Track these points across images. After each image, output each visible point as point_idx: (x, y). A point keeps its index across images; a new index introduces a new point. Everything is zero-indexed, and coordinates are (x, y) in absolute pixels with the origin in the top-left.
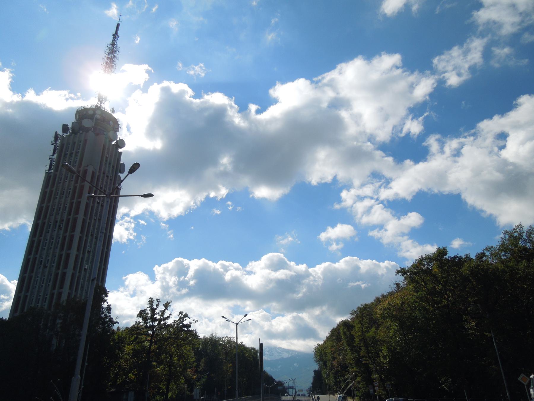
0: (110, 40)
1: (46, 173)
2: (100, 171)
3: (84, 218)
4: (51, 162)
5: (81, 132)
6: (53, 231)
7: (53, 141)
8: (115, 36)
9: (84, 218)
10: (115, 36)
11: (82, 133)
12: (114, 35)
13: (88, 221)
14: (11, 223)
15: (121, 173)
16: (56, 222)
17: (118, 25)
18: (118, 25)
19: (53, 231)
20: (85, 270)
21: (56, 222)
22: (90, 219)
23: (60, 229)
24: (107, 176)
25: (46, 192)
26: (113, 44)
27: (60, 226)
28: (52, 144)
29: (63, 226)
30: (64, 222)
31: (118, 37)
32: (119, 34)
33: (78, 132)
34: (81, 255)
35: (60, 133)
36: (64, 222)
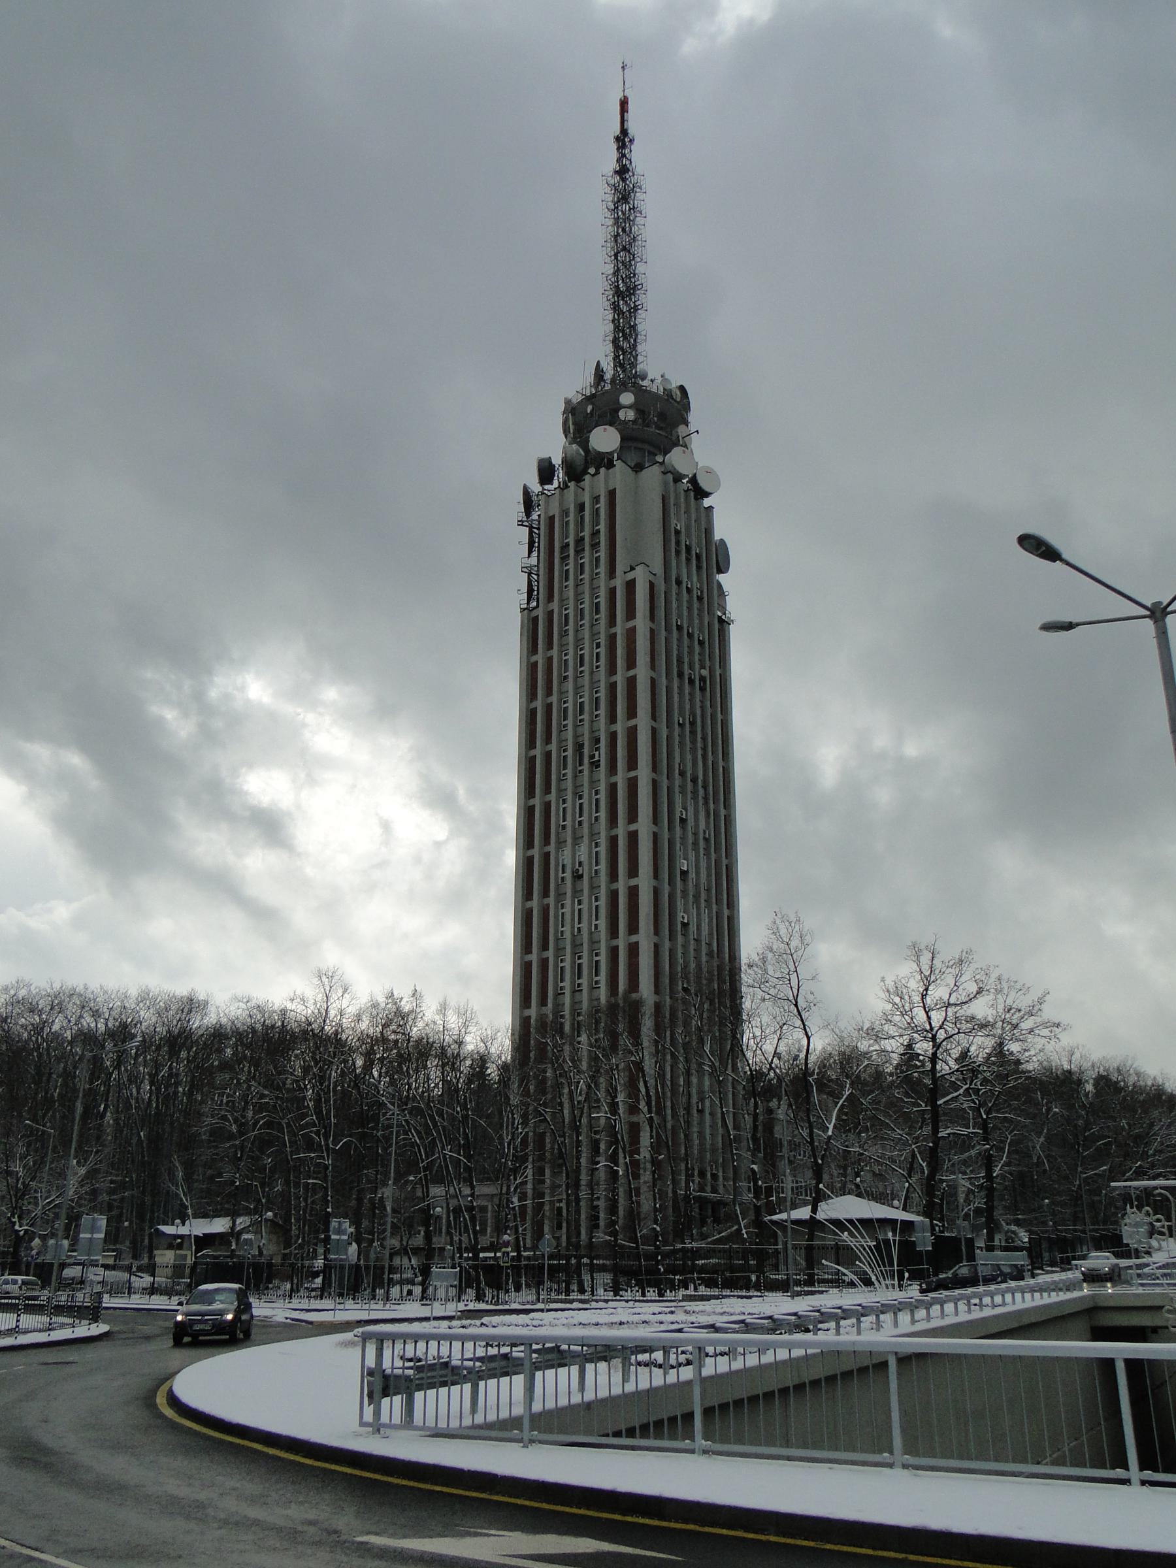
0: (609, 160)
1: (523, 610)
2: (667, 579)
3: (655, 829)
4: (530, 574)
5: (592, 470)
6: (577, 774)
7: (523, 516)
8: (623, 140)
9: (655, 829)
10: (623, 140)
11: (597, 473)
12: (617, 139)
13: (665, 781)
14: (646, 1017)
15: (720, 571)
16: (579, 747)
17: (624, 104)
18: (624, 104)
19: (577, 774)
20: (684, 874)
21: (579, 747)
22: (669, 725)
23: (595, 765)
24: (689, 590)
25: (535, 665)
26: (623, 171)
27: (592, 756)
28: (521, 523)
29: (602, 756)
30: (603, 744)
31: (631, 141)
32: (632, 131)
33: (585, 472)
34: (666, 889)
35: (536, 487)
36: (603, 744)
